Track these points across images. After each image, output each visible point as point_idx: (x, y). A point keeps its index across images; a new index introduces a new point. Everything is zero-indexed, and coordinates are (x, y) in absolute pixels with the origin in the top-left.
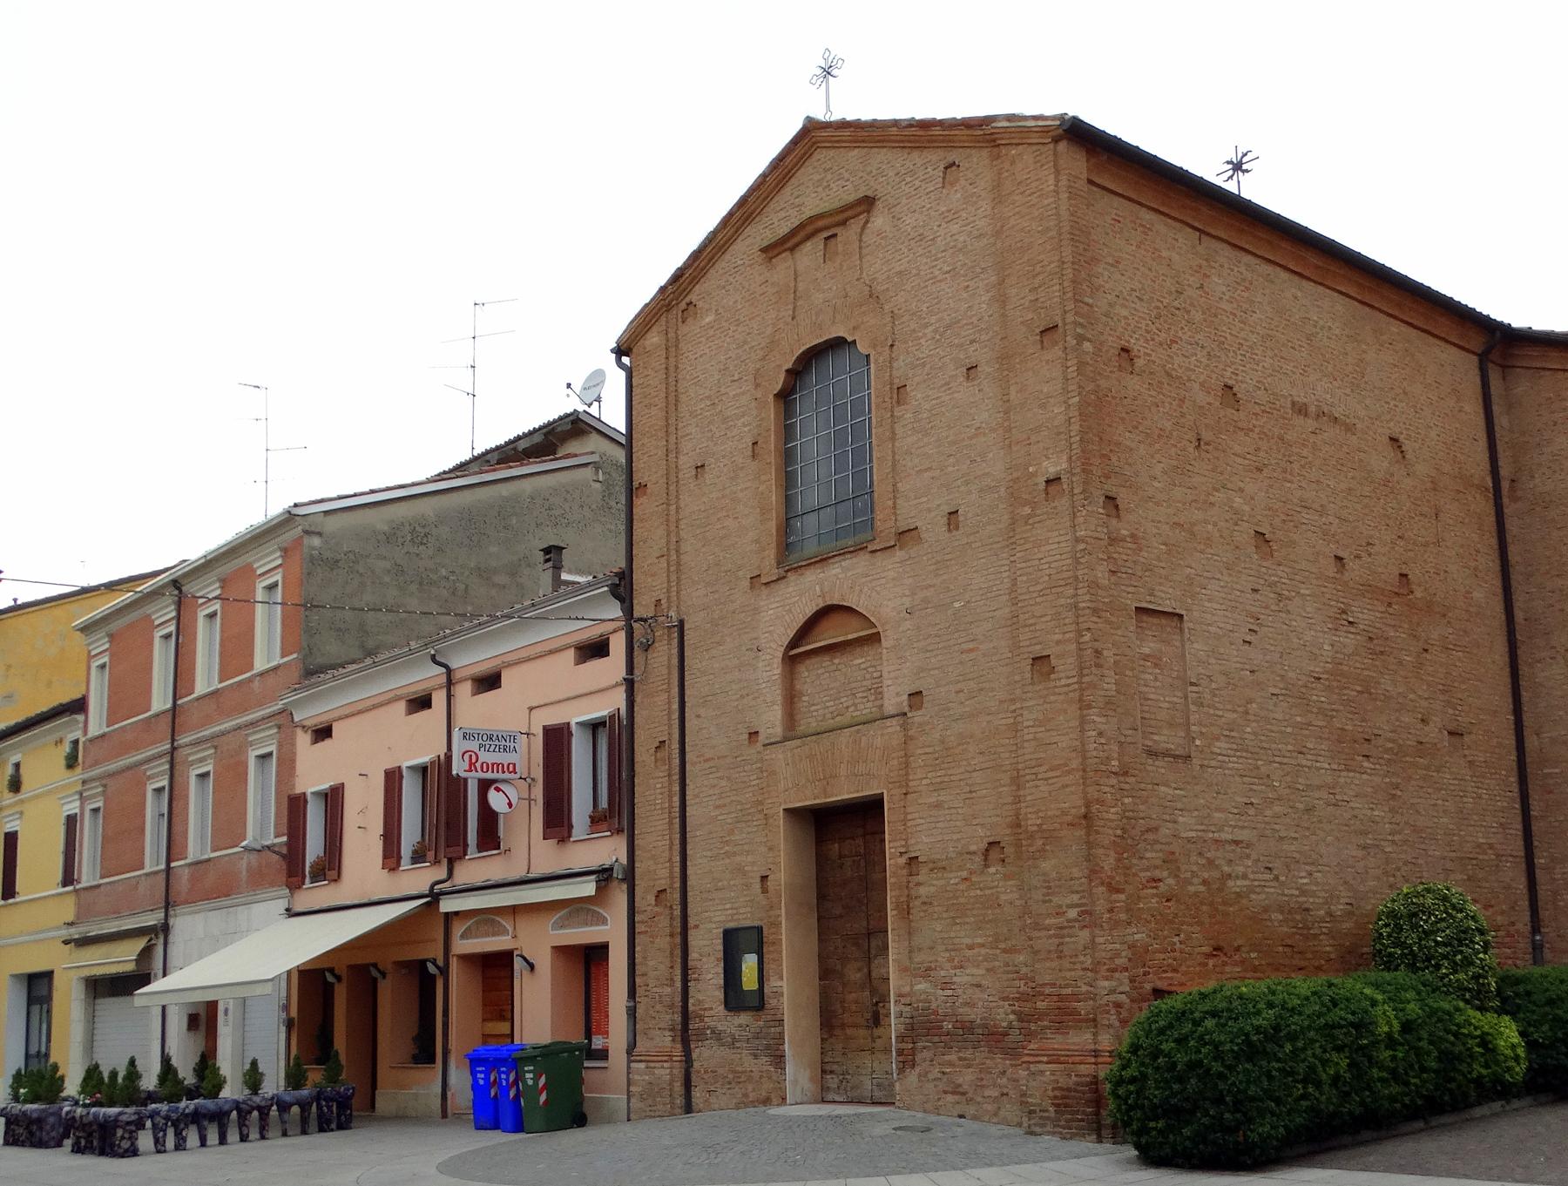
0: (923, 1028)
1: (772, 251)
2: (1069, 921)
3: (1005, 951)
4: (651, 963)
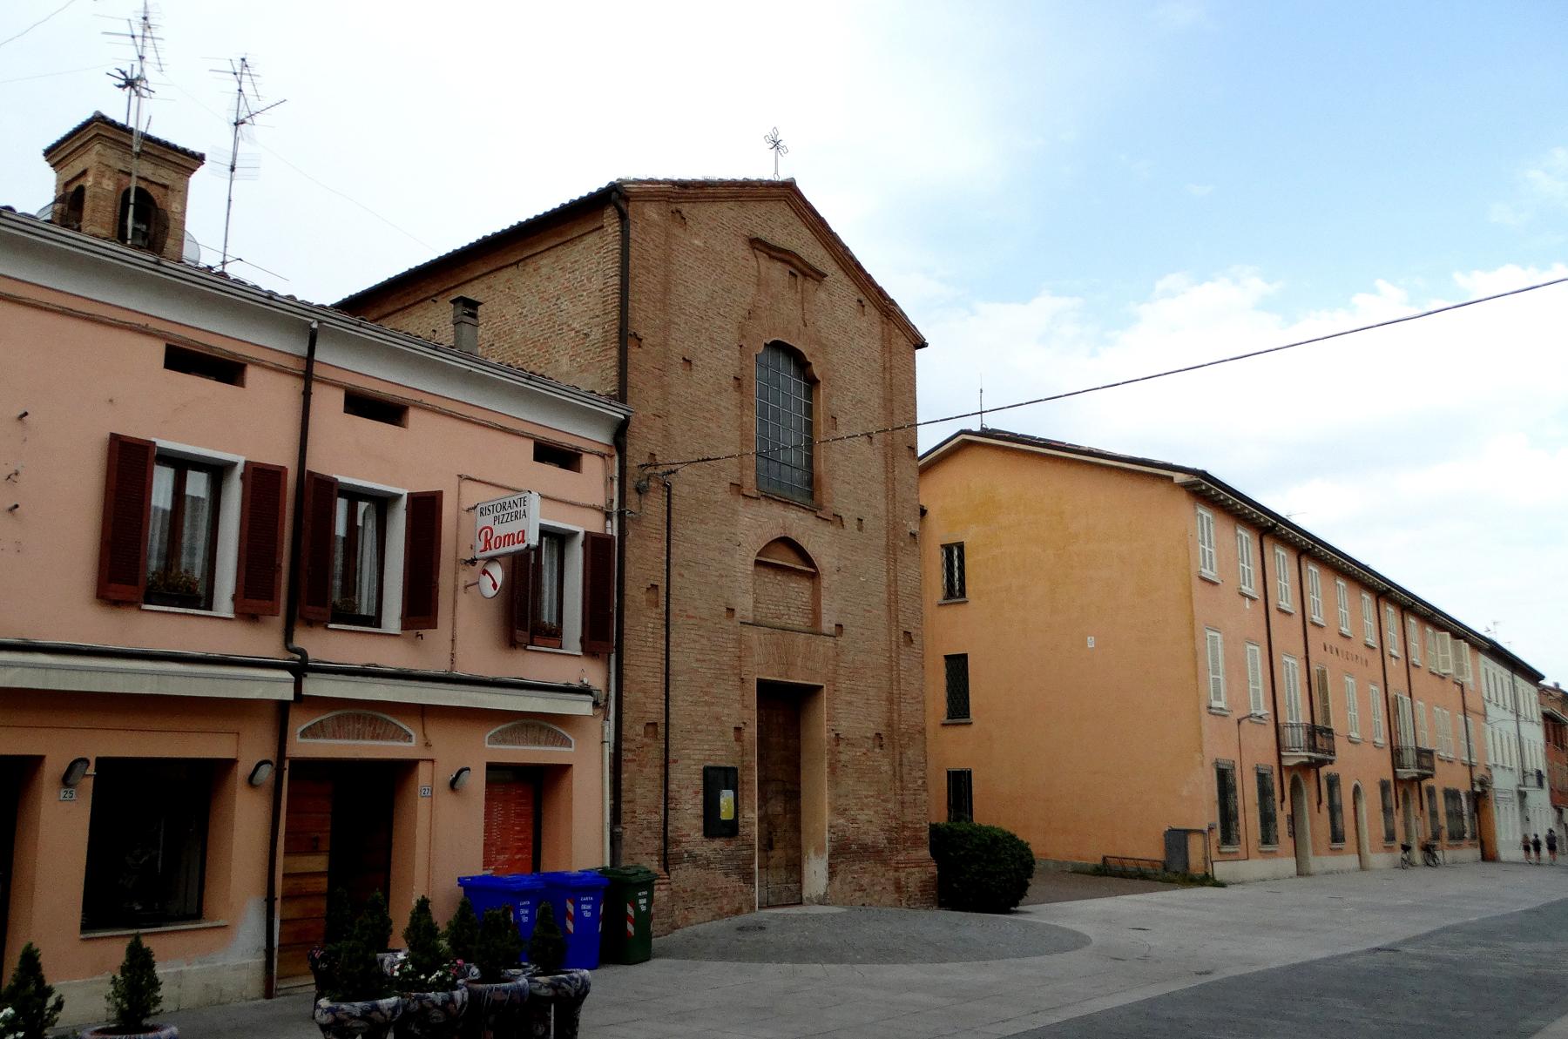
1: (756, 243)
4: (639, 791)
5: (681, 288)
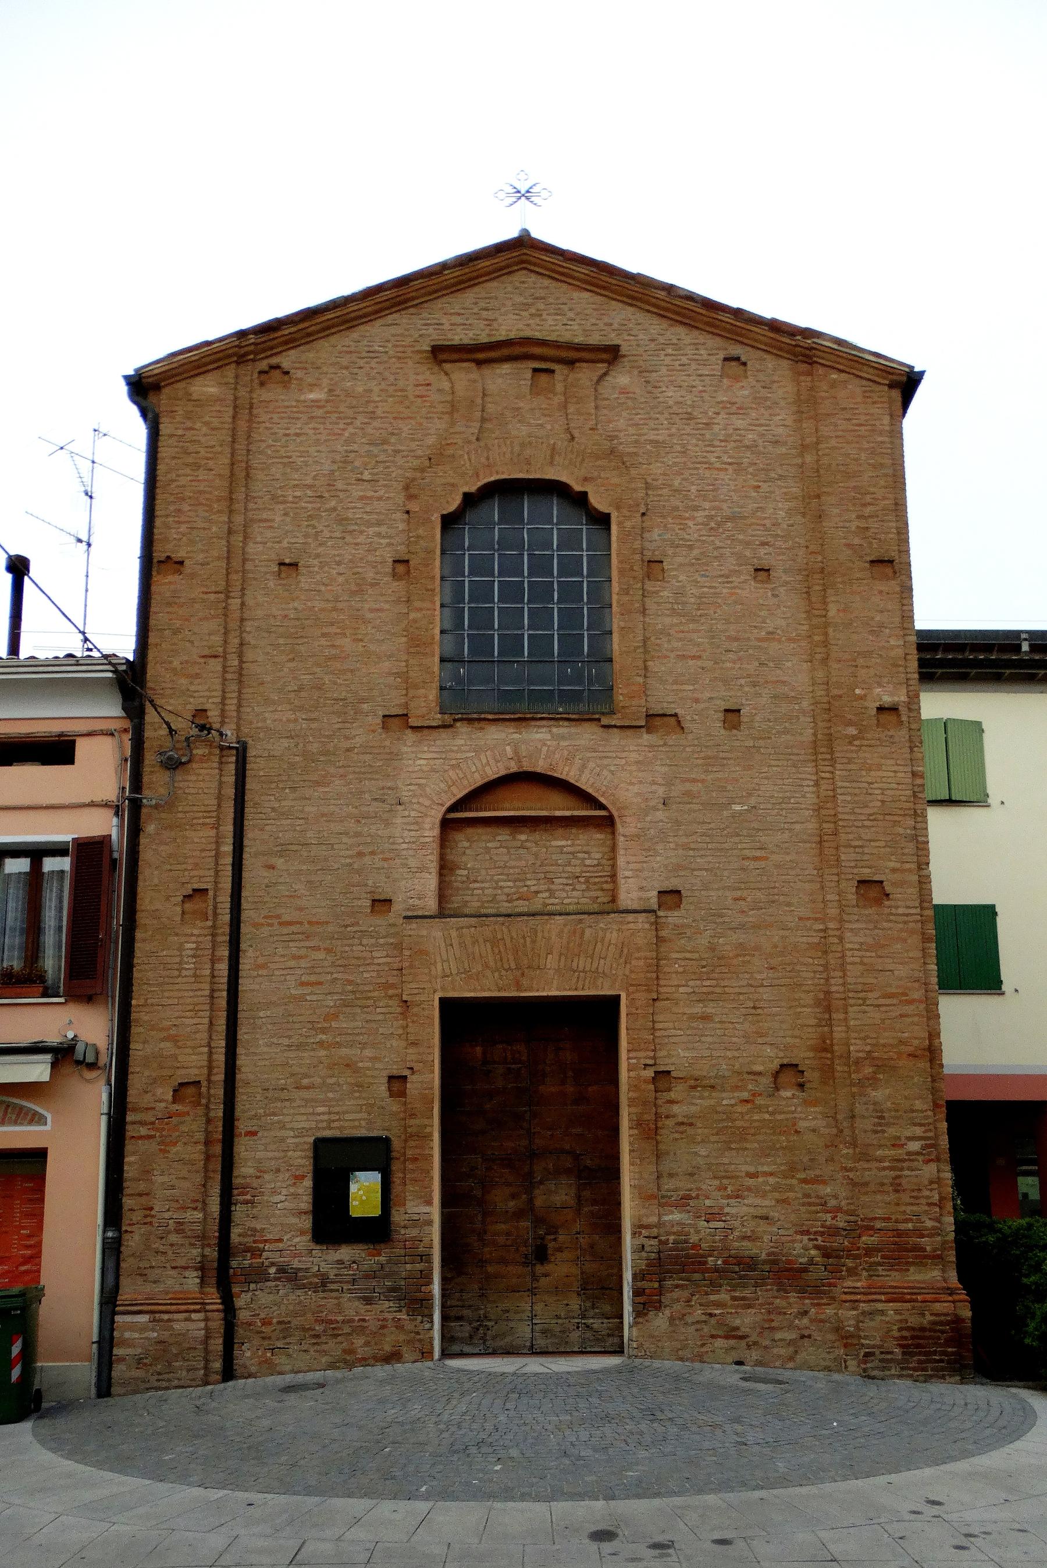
0: (674, 1266)
1: (442, 354)
2: (909, 1153)
3: (804, 1181)
5: (276, 471)
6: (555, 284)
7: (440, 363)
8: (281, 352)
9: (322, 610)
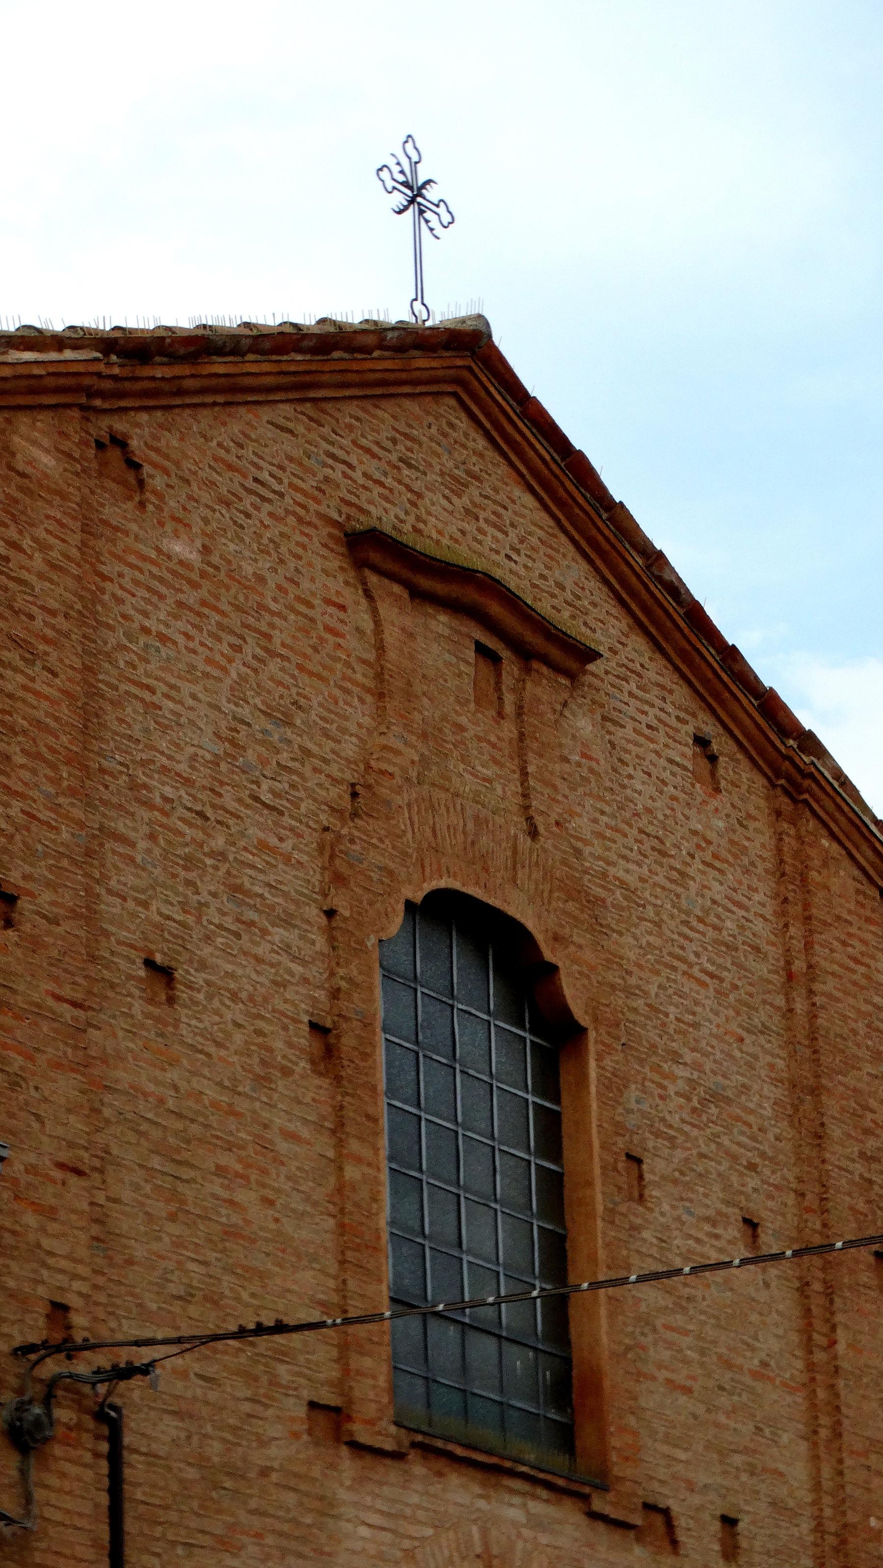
1: (371, 551)
6: (491, 454)
7: (360, 564)
8: (126, 410)
9: (215, 1104)
